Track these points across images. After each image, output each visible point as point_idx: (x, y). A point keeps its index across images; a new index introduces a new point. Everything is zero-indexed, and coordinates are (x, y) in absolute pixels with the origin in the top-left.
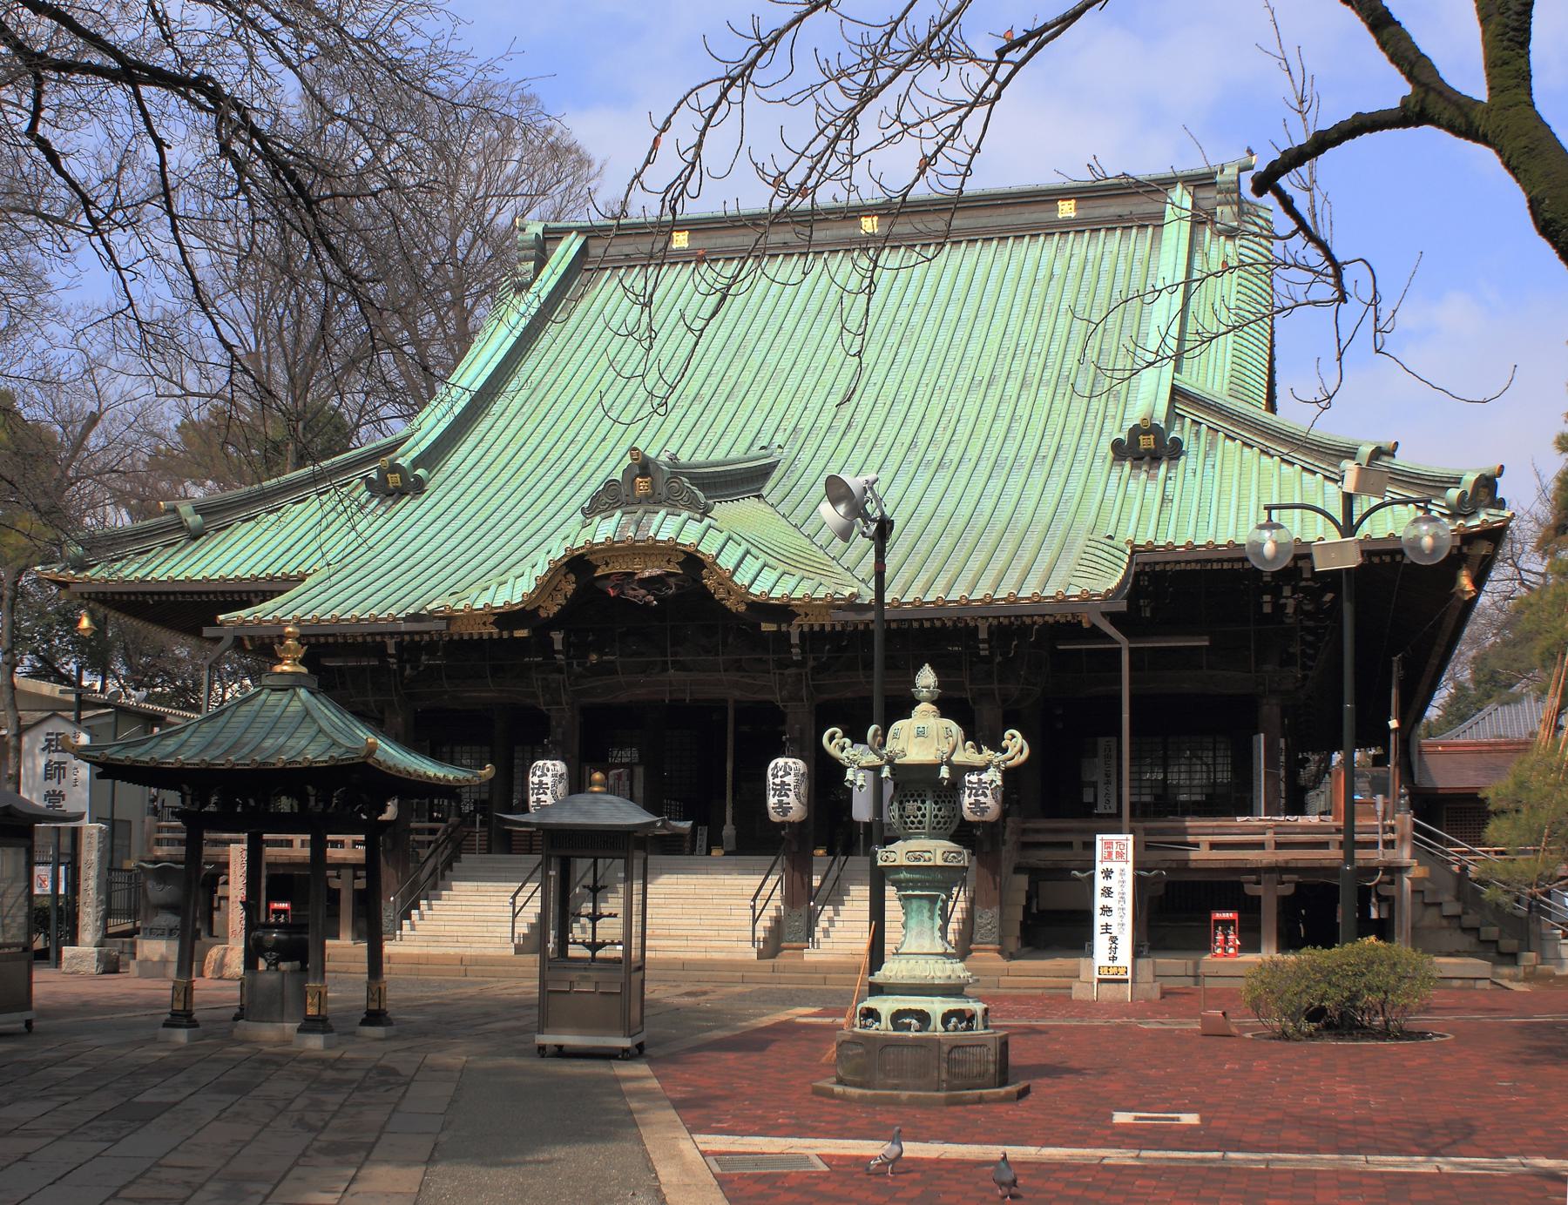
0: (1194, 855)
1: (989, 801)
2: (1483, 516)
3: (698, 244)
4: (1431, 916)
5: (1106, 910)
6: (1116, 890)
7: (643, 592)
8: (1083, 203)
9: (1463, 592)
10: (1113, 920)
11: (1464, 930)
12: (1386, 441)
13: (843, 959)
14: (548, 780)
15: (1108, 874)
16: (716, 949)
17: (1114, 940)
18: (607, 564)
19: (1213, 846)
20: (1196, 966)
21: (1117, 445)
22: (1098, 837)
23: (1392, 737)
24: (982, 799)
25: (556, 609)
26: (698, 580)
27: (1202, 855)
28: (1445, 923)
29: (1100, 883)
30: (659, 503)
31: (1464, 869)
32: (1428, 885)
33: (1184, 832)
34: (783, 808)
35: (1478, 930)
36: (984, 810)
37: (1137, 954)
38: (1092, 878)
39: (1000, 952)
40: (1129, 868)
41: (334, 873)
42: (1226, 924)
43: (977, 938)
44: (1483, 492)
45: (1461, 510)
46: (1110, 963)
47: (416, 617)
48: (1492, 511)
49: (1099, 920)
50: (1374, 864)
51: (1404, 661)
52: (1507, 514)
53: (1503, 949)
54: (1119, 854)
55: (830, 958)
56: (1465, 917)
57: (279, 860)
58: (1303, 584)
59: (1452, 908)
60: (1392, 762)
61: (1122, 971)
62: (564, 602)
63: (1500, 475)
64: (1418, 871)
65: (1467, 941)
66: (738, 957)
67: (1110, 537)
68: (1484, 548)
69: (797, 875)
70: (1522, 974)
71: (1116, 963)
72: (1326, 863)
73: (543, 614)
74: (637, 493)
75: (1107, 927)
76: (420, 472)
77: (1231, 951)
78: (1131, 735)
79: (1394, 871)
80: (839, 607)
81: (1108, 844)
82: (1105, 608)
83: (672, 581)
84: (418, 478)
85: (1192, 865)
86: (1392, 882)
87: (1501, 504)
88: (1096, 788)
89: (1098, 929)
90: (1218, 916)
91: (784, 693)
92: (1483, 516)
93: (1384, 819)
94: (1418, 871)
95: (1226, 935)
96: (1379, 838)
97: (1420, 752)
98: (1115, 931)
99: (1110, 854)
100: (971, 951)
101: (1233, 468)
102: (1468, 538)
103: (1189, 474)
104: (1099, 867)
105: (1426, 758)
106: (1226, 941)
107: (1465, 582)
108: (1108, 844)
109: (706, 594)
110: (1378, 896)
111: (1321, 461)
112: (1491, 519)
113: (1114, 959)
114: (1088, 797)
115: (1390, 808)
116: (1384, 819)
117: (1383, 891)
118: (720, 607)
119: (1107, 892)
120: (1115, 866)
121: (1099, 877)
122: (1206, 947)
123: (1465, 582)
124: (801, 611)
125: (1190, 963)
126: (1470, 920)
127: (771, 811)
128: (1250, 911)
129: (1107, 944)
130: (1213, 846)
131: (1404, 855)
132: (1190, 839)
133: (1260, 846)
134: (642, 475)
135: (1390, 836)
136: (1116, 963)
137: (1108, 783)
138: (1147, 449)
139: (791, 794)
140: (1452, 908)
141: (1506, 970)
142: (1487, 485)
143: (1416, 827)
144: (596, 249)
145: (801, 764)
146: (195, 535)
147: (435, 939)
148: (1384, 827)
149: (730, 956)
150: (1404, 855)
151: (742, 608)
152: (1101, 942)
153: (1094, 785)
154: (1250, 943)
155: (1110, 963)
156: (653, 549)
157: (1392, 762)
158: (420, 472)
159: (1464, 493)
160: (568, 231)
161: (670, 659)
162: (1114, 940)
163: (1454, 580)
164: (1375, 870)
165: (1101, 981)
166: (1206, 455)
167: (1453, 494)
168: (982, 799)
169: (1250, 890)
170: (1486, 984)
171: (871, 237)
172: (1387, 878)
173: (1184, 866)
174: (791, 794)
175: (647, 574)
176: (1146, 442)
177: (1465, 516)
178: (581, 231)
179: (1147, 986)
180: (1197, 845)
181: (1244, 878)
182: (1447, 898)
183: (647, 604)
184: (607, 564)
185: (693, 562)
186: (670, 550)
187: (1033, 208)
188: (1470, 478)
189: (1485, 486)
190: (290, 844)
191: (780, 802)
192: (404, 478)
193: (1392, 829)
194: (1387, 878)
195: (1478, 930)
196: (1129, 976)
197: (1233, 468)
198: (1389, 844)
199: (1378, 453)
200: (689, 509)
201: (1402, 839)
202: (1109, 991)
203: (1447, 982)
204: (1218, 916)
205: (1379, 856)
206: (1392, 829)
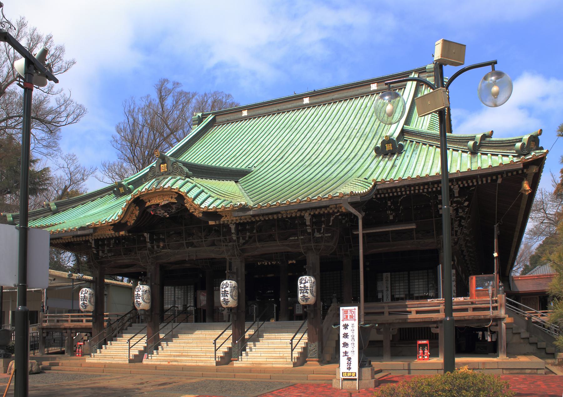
0: (409, 316)
1: (309, 295)
2: (533, 153)
3: (250, 114)
4: (516, 339)
5: (346, 345)
6: (350, 334)
7: (163, 211)
8: (379, 84)
9: (525, 191)
10: (348, 349)
11: (531, 344)
12: (487, 132)
13: (249, 365)
14: (140, 293)
15: (346, 326)
16: (202, 361)
17: (349, 359)
18: (150, 201)
19: (418, 312)
20: (409, 365)
21: (377, 149)
22: (341, 308)
23: (495, 261)
24: (306, 294)
25: (133, 222)
26: (183, 205)
27: (413, 316)
28: (522, 341)
29: (342, 331)
30: (169, 174)
31: (530, 318)
32: (514, 325)
33: (406, 306)
34: (227, 302)
35: (537, 343)
36: (307, 299)
37: (362, 364)
38: (339, 329)
39: (318, 361)
40: (356, 323)
41: (65, 331)
42: (423, 346)
43: (309, 356)
44: (533, 144)
45: (521, 153)
46: (348, 371)
47: (82, 228)
48: (537, 151)
49: (342, 349)
50: (488, 317)
51: (499, 226)
52: (545, 151)
53: (548, 352)
54: (351, 317)
55: (244, 365)
56: (530, 338)
57: (78, 327)
58: (455, 199)
59: (525, 335)
60: (495, 272)
61: (354, 375)
62: (135, 218)
63: (540, 134)
64: (508, 320)
65: (532, 348)
66: (209, 364)
67: (365, 179)
68: (534, 169)
69: (237, 330)
70: (557, 362)
71: (351, 371)
72: (466, 318)
73: (129, 224)
74: (162, 171)
75: (346, 353)
76: (130, 186)
77: (426, 357)
78: (358, 256)
79: (497, 320)
80: (236, 210)
81: (346, 312)
82: (349, 200)
83: (174, 206)
84: (129, 188)
85: (409, 321)
86: (497, 325)
87: (542, 148)
88: (383, 293)
89: (342, 354)
90: (420, 342)
91: (229, 253)
92: (533, 153)
93: (492, 297)
94: (508, 320)
95: (423, 351)
96: (490, 306)
97: (513, 280)
98: (350, 355)
99: (347, 316)
100: (306, 362)
101: (424, 153)
102: (527, 165)
103: (406, 156)
104: (342, 323)
105: (516, 282)
106: (424, 353)
107: (526, 186)
108: (346, 312)
109: (186, 210)
110: (491, 331)
111: (461, 145)
112: (537, 155)
113: (349, 368)
114: (380, 296)
115: (495, 292)
116: (492, 297)
117: (493, 329)
118: (192, 215)
119: (346, 336)
120: (349, 322)
121: (342, 328)
122: (414, 355)
123: (526, 186)
124: (224, 215)
125: (406, 364)
126: (532, 340)
127: (222, 303)
128: (433, 338)
129: (346, 361)
130: (418, 312)
131: (502, 313)
132: (408, 309)
133: (438, 311)
134: (163, 163)
135: (495, 305)
136: (351, 371)
137: (387, 290)
138: (389, 149)
139: (229, 295)
140: (525, 335)
141: (550, 361)
142: (534, 140)
143: (507, 301)
144: (219, 119)
145: (234, 283)
146: (55, 212)
147: (105, 357)
148: (492, 301)
149: (206, 364)
150: (502, 313)
151: (201, 215)
152: (343, 360)
153: (382, 292)
154: (434, 354)
155: (348, 371)
156: (163, 192)
157: (495, 272)
158: (130, 186)
159: (523, 144)
160: (209, 114)
161: (184, 242)
162: (349, 359)
163: (521, 185)
164: (489, 320)
165: (344, 379)
166: (414, 150)
167: (518, 145)
168: (306, 294)
169: (434, 331)
170: (543, 372)
171: (307, 105)
172: (494, 323)
173: (405, 321)
174: (229, 295)
175: (163, 203)
176: (389, 147)
177: (525, 155)
178: (213, 114)
179: (367, 382)
180: (410, 312)
181: (431, 326)
182: (522, 330)
183: (165, 216)
184: (150, 201)
185: (181, 197)
186: (170, 192)
187: (362, 88)
188: (526, 137)
189: (533, 141)
190: (82, 321)
191: (224, 299)
192: (125, 189)
193: (496, 302)
194: (494, 323)
195: (537, 343)
196: (357, 377)
197: (424, 153)
198: (495, 308)
199: (484, 137)
200: (181, 175)
201: (501, 305)
202: (347, 384)
203: (523, 371)
204: (420, 342)
205: (490, 313)
206: (496, 302)
